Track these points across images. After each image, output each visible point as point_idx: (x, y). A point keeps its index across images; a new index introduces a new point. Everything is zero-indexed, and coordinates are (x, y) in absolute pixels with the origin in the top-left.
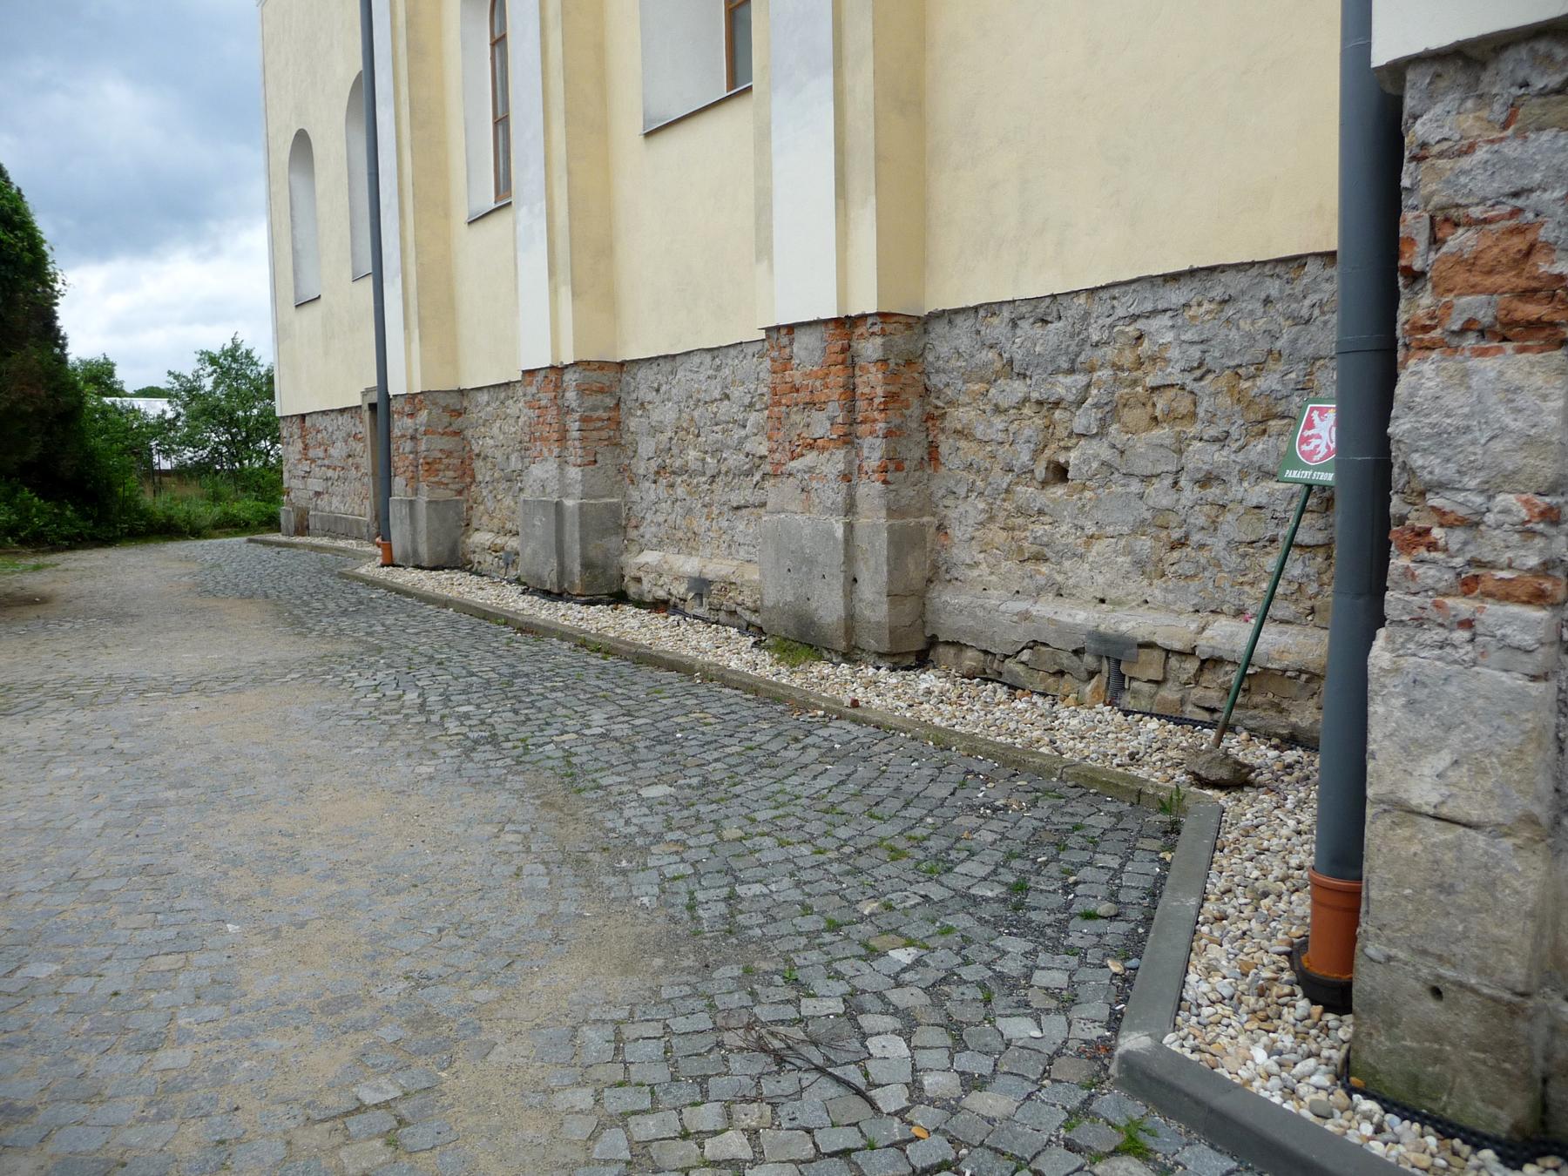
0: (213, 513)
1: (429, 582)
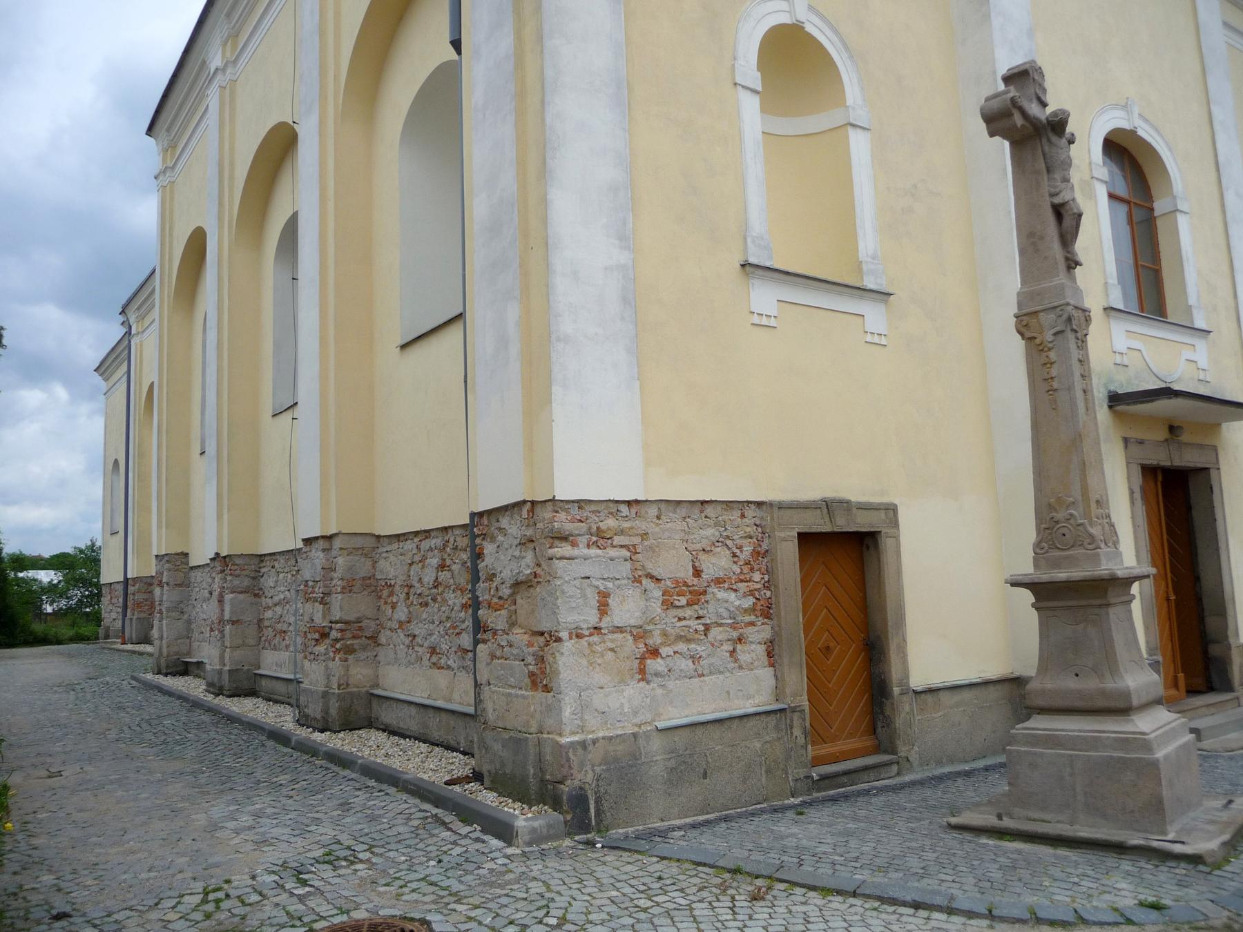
0: (71, 633)
1: (137, 648)
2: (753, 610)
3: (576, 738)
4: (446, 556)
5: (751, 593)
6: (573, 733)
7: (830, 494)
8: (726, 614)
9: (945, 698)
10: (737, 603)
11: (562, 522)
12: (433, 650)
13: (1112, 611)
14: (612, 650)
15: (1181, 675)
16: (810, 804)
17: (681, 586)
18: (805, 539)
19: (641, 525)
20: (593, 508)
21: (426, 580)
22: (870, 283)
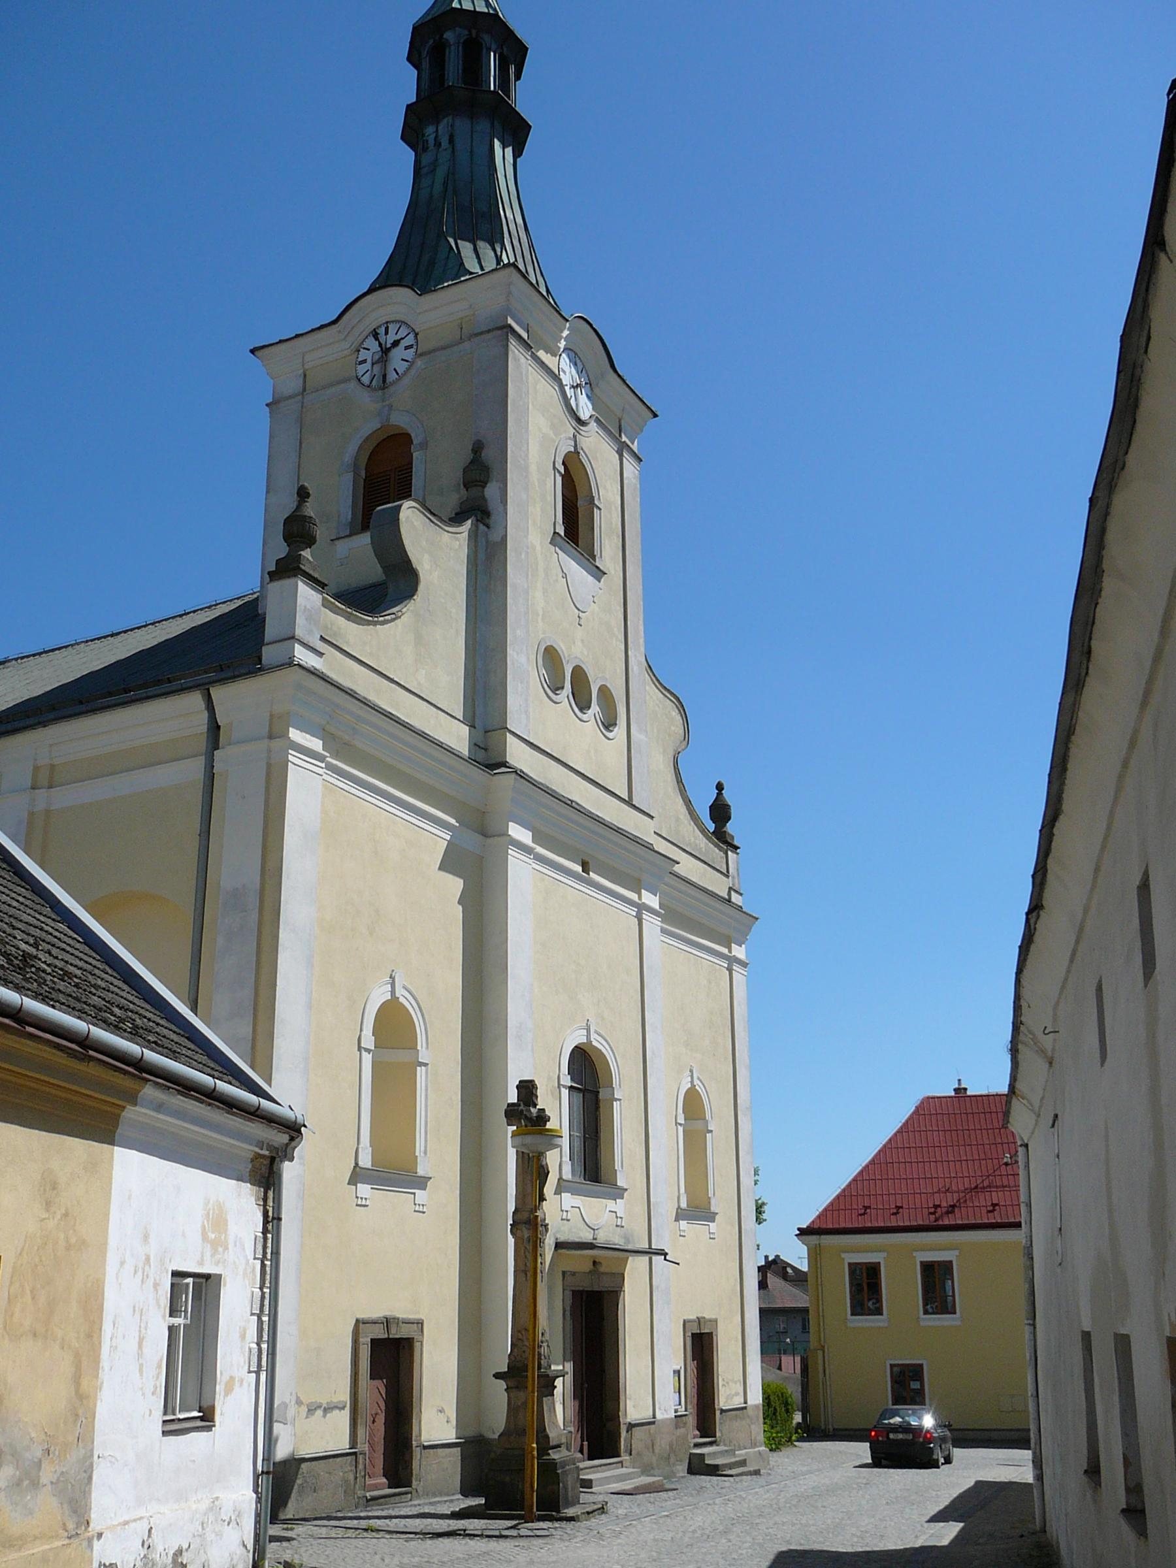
7: (388, 1313)
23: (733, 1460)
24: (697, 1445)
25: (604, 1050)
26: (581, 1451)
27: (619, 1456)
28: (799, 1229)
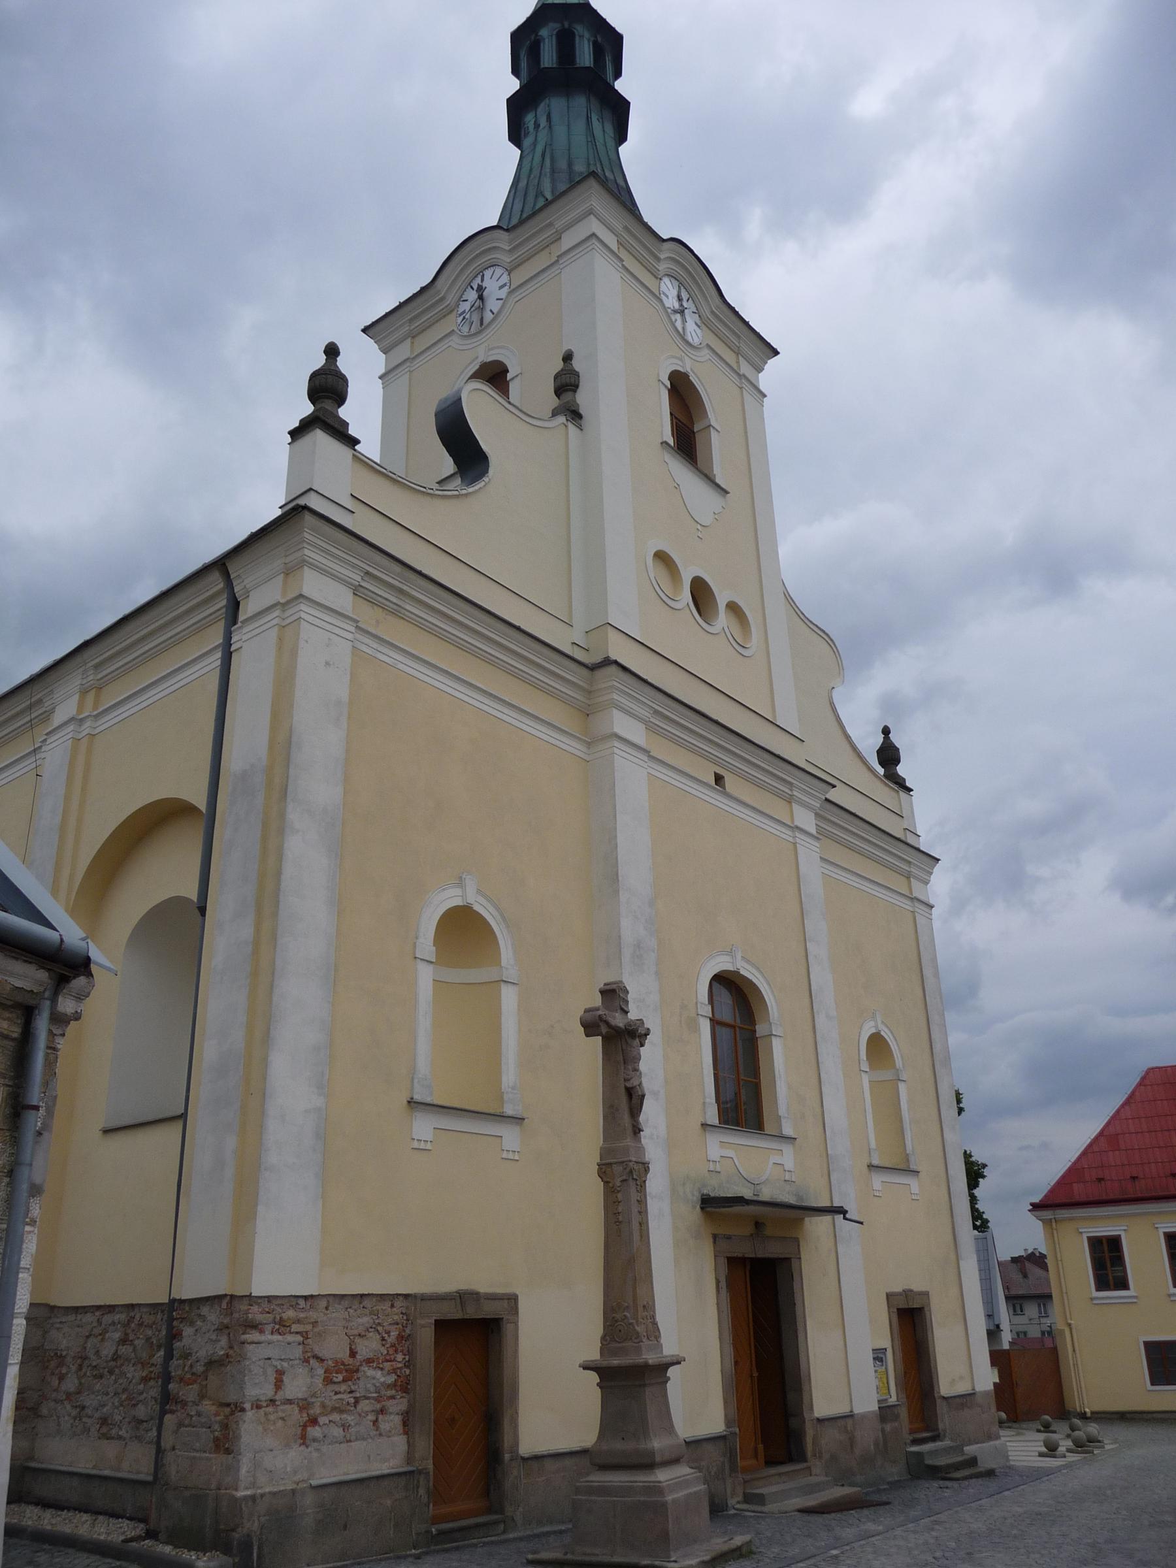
2: (394, 1385)
3: (249, 1493)
4: (129, 1331)
5: (394, 1371)
6: (247, 1488)
7: (463, 1287)
8: (372, 1389)
9: (549, 1465)
10: (382, 1380)
11: (255, 1313)
12: (104, 1421)
13: (648, 1390)
14: (283, 1419)
15: (761, 1446)
16: (427, 1553)
17: (339, 1366)
18: (442, 1326)
19: (313, 1315)
20: (279, 1302)
21: (104, 1353)
22: (509, 1110)
23: (960, 1459)
24: (915, 1442)
25: (755, 980)
26: (756, 1457)
27: (806, 1461)
28: (1032, 1204)
